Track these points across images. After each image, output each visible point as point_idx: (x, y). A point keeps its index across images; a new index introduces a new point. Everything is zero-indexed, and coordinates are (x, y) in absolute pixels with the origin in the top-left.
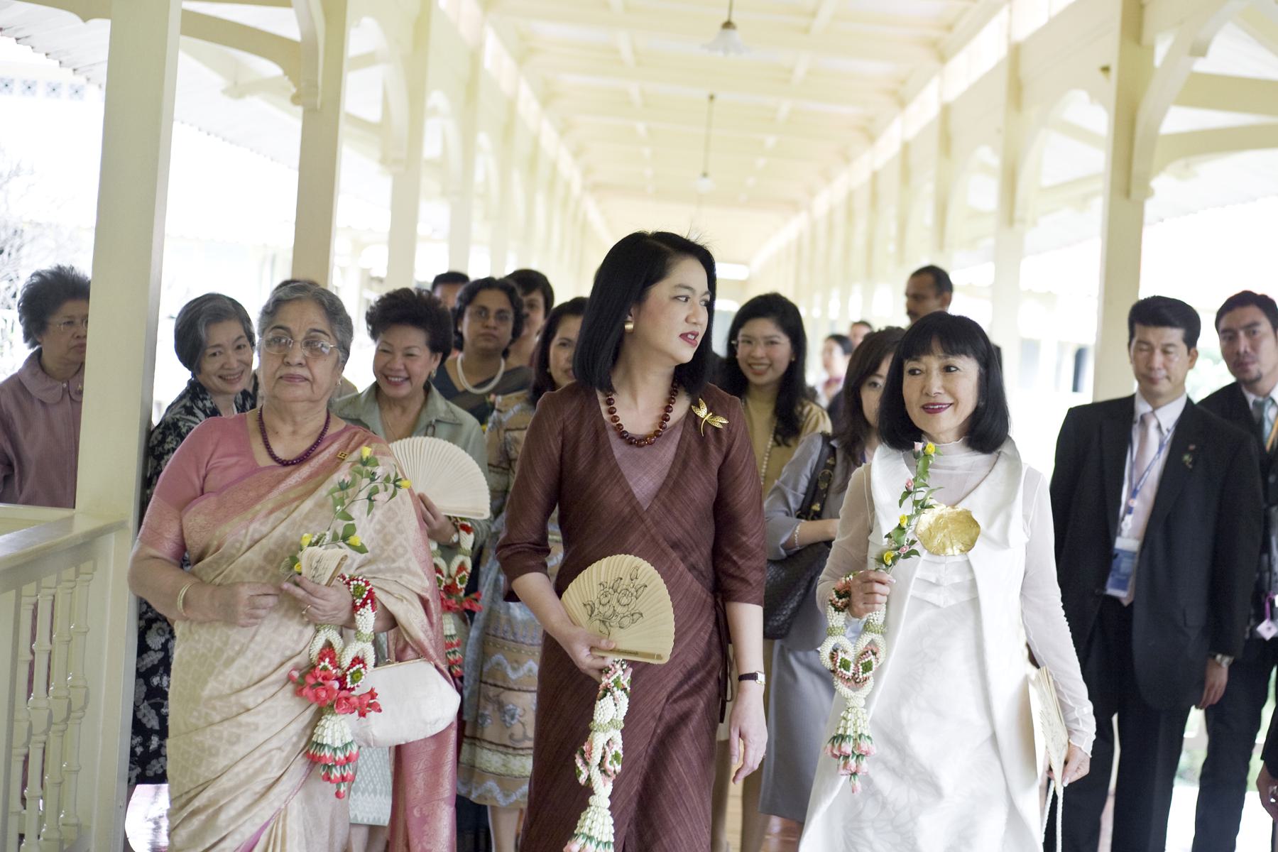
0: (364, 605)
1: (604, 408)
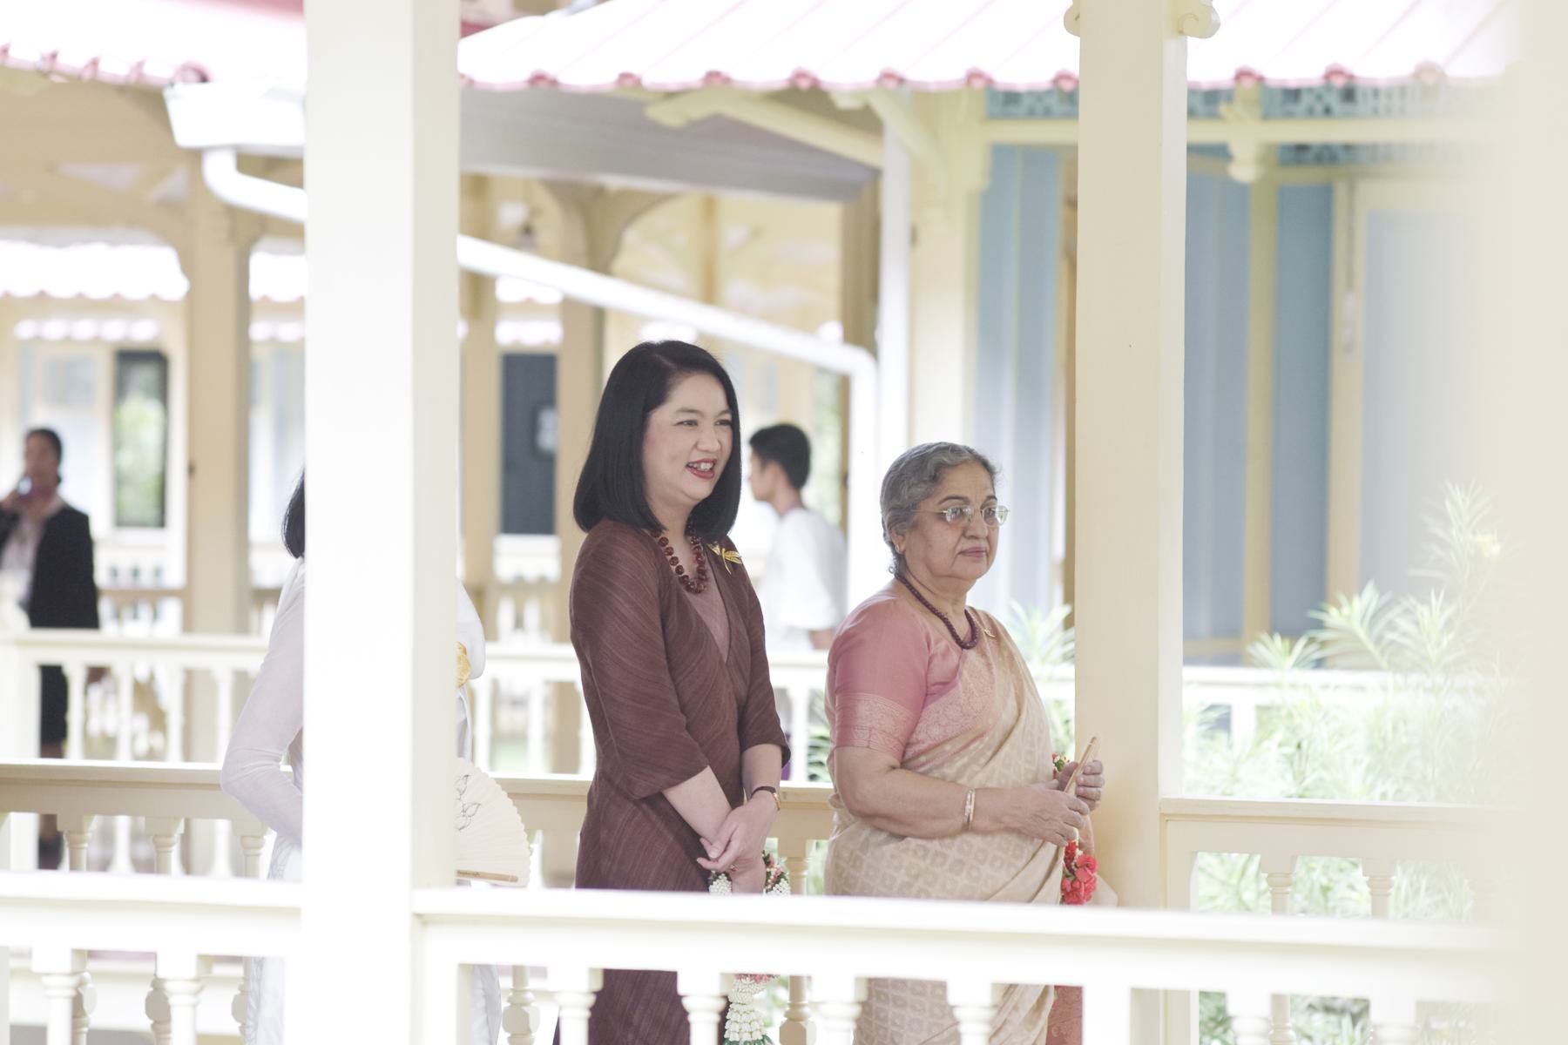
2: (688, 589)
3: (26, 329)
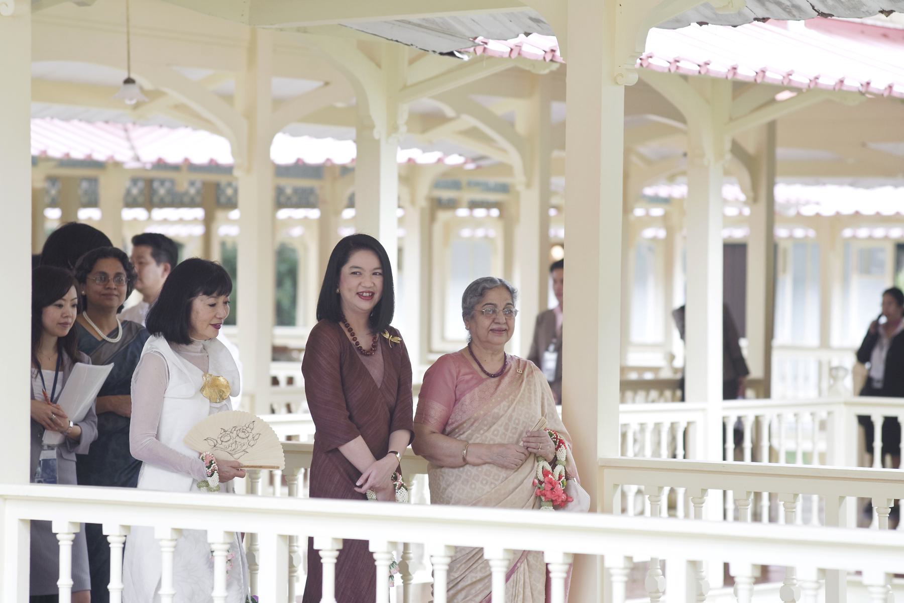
2: (362, 353)
3: (848, 233)
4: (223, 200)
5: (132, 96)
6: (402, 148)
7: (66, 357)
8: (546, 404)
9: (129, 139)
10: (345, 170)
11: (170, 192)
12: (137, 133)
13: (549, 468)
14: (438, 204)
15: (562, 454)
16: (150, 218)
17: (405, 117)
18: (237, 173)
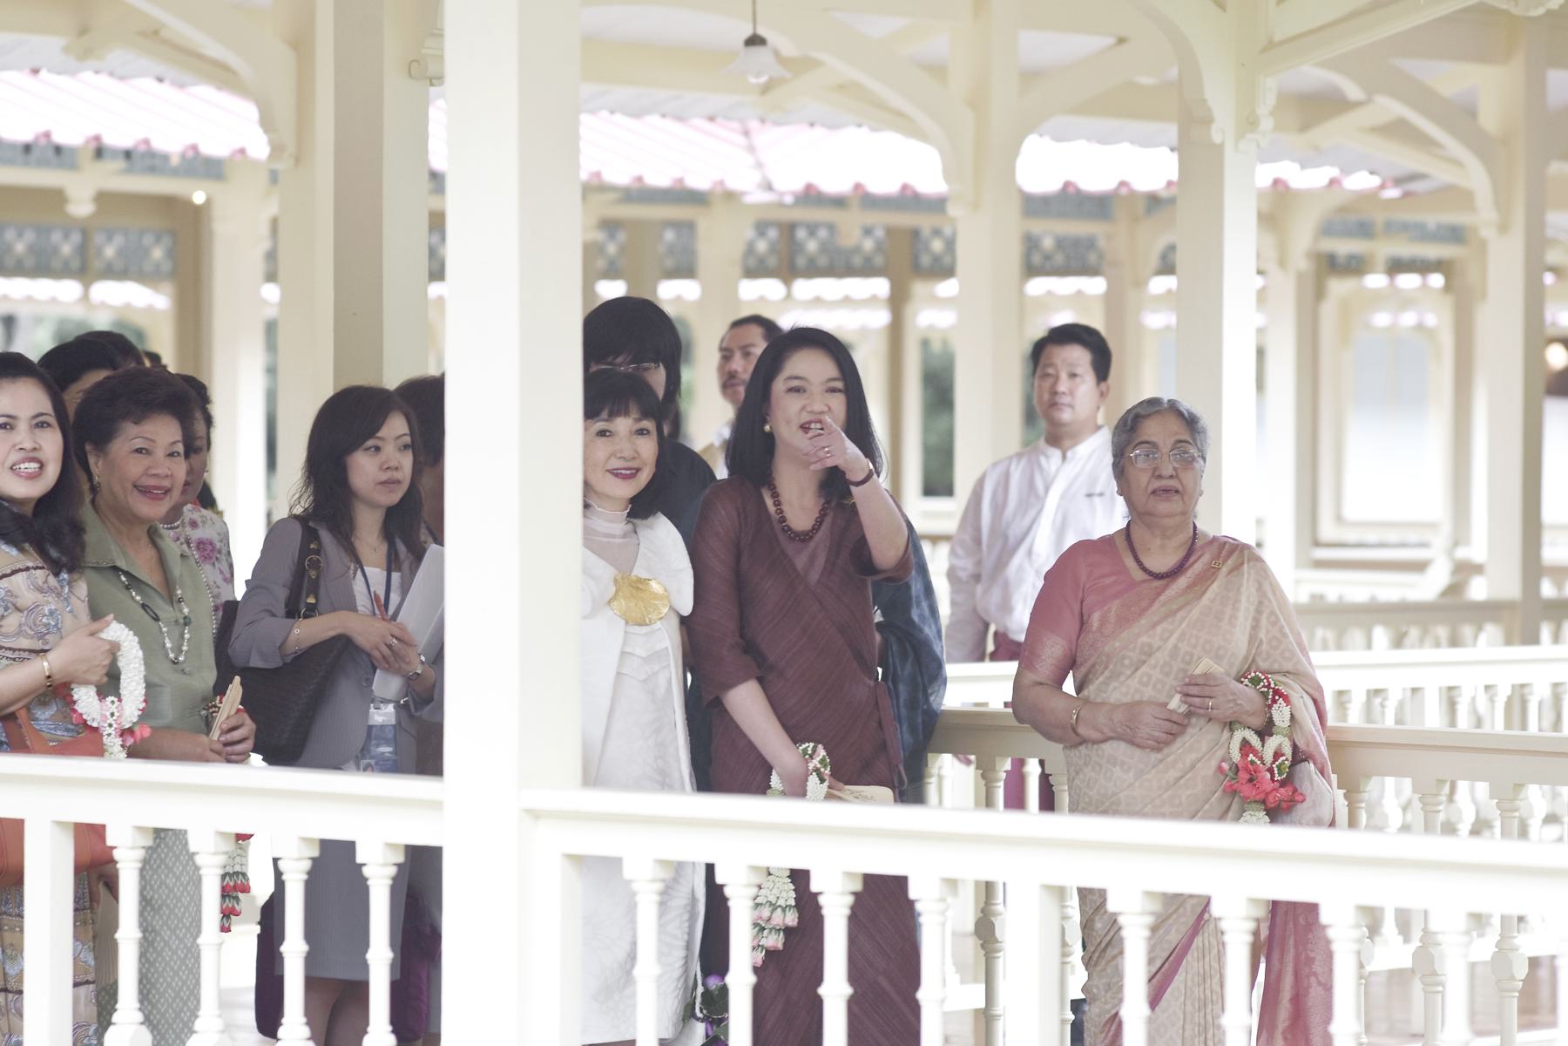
0: (1274, 701)
1: (769, 502)
4: (925, 260)
5: (760, 65)
6: (1262, 162)
7: (402, 548)
8: (1264, 621)
9: (751, 149)
10: (1154, 202)
11: (824, 248)
12: (765, 136)
13: (1255, 740)
14: (1331, 266)
15: (1281, 714)
16: (789, 295)
17: (1271, 100)
18: (953, 210)
